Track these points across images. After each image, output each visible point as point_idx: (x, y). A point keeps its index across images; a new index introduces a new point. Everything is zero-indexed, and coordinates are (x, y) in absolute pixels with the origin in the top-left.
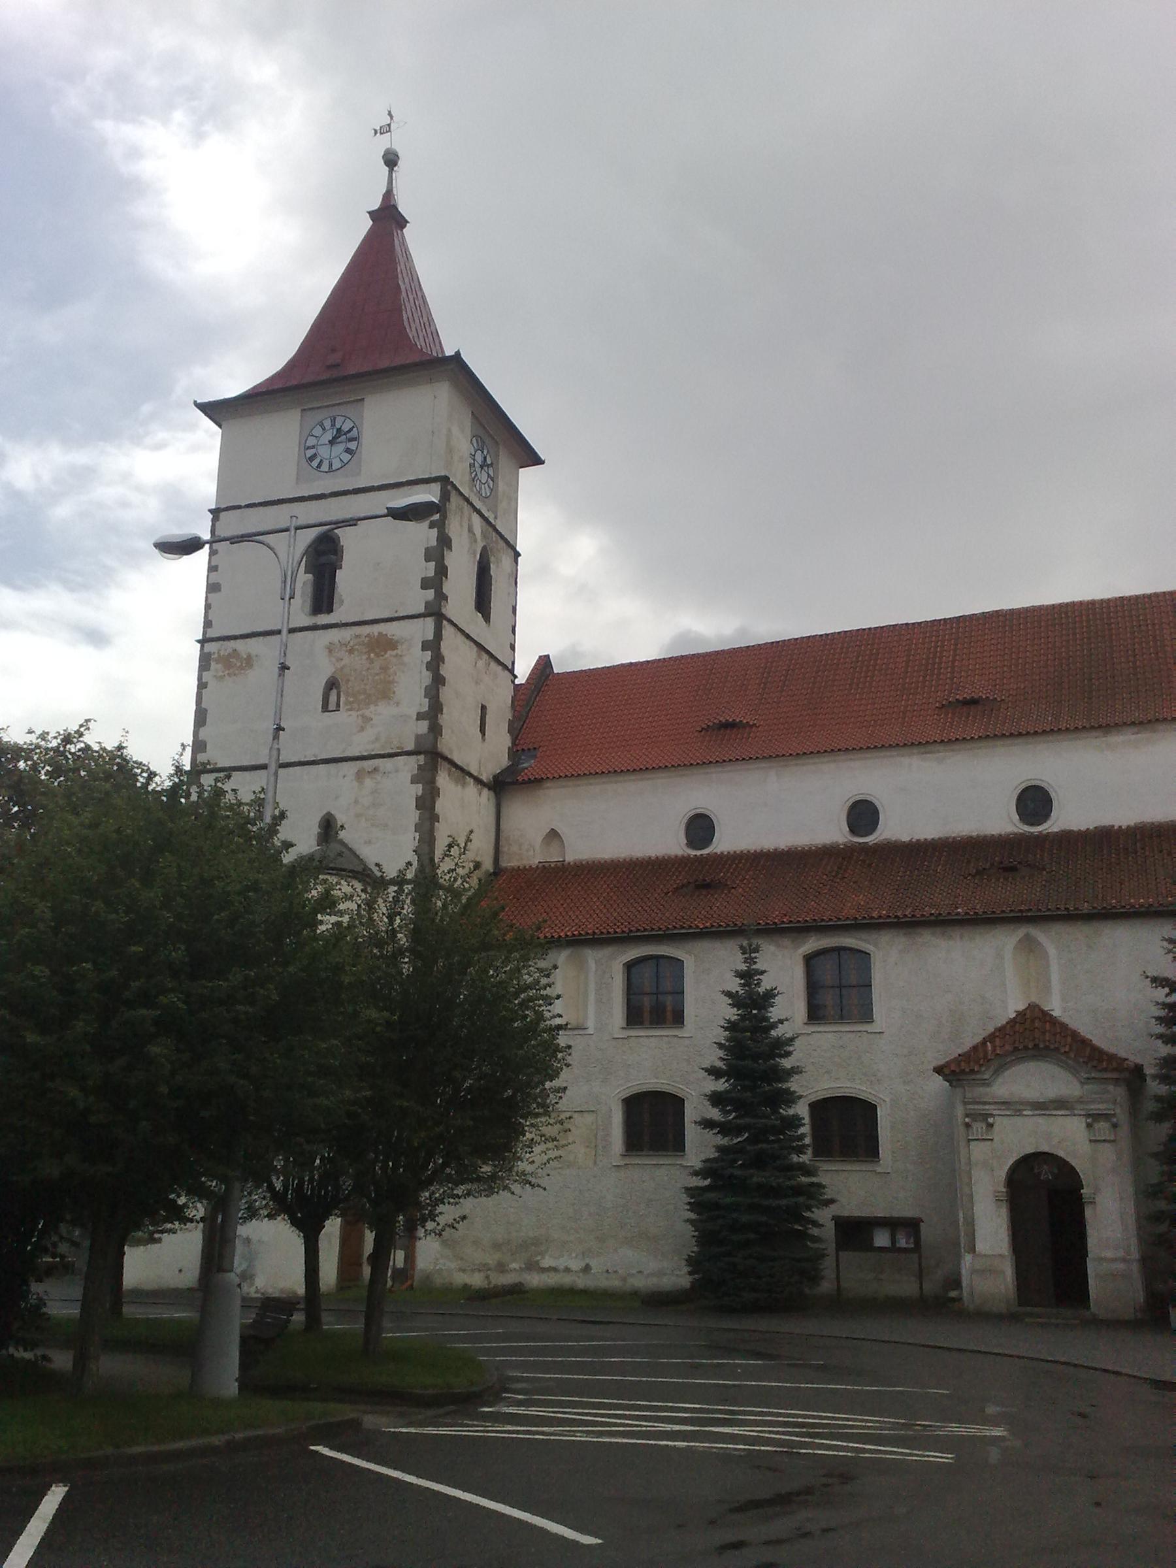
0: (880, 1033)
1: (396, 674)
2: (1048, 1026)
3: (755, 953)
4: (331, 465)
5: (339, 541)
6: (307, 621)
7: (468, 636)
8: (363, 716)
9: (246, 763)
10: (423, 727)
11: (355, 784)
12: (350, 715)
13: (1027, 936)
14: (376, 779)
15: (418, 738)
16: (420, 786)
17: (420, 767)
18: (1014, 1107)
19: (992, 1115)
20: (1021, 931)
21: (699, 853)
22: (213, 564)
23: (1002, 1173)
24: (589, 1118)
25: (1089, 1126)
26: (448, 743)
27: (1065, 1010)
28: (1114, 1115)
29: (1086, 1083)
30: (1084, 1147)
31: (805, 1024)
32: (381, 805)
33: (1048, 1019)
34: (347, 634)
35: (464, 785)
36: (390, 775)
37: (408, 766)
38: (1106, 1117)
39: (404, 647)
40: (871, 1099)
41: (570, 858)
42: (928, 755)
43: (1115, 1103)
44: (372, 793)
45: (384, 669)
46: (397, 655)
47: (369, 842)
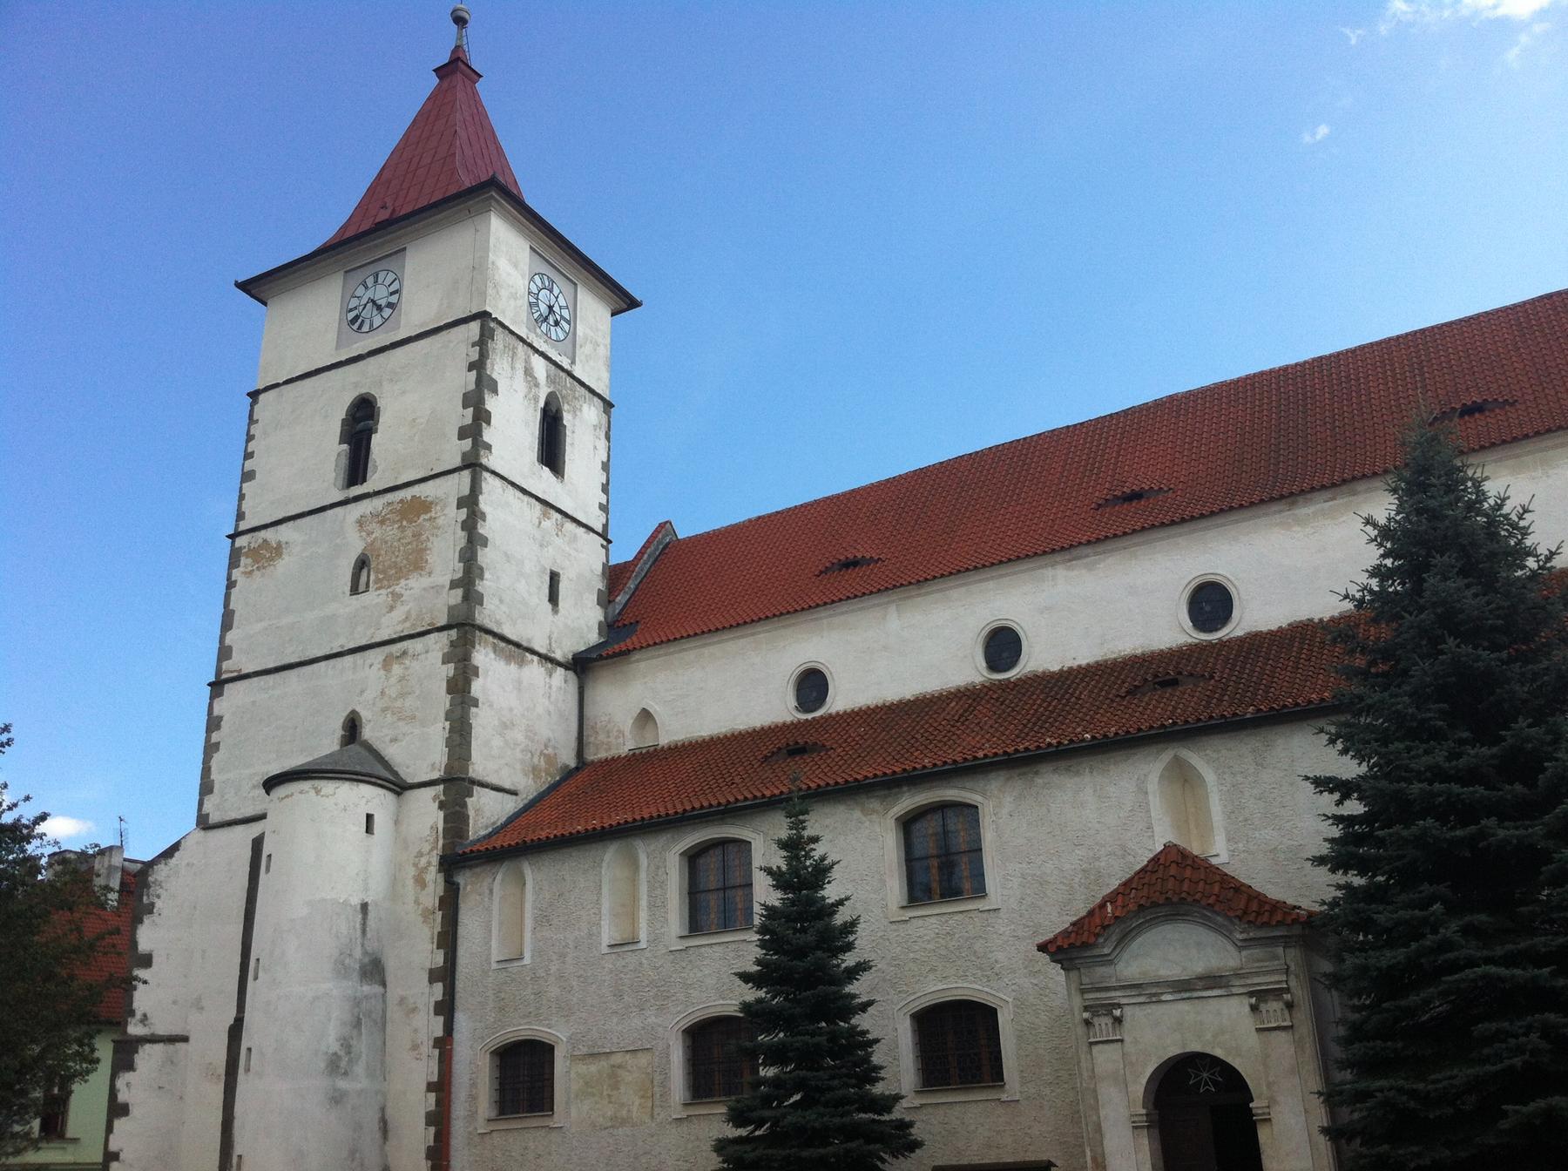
0: (995, 910)
1: (429, 540)
2: (1188, 873)
3: (803, 815)
4: (371, 325)
5: (376, 402)
6: (338, 496)
7: (524, 491)
8: (392, 593)
9: (271, 665)
10: (457, 596)
11: (382, 672)
12: (379, 595)
13: (1176, 758)
14: (404, 664)
15: (451, 609)
16: (452, 666)
17: (452, 644)
18: (1149, 991)
19: (1119, 1006)
20: (1167, 755)
21: (810, 716)
22: (249, 450)
23: (1138, 1088)
24: (643, 1060)
25: (1254, 1008)
26: (491, 613)
27: (1232, 853)
28: (1288, 990)
29: (1244, 948)
30: (1252, 1040)
31: (903, 908)
32: (410, 694)
33: (1189, 862)
34: (377, 504)
35: (521, 663)
36: (420, 657)
37: (438, 644)
38: (1277, 993)
39: (438, 508)
40: (990, 1001)
41: (664, 740)
42: (1074, 562)
43: (1287, 971)
44: (400, 681)
45: (417, 535)
46: (431, 518)
47: (394, 740)
